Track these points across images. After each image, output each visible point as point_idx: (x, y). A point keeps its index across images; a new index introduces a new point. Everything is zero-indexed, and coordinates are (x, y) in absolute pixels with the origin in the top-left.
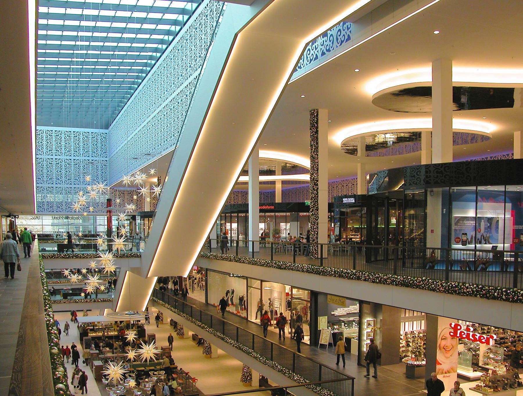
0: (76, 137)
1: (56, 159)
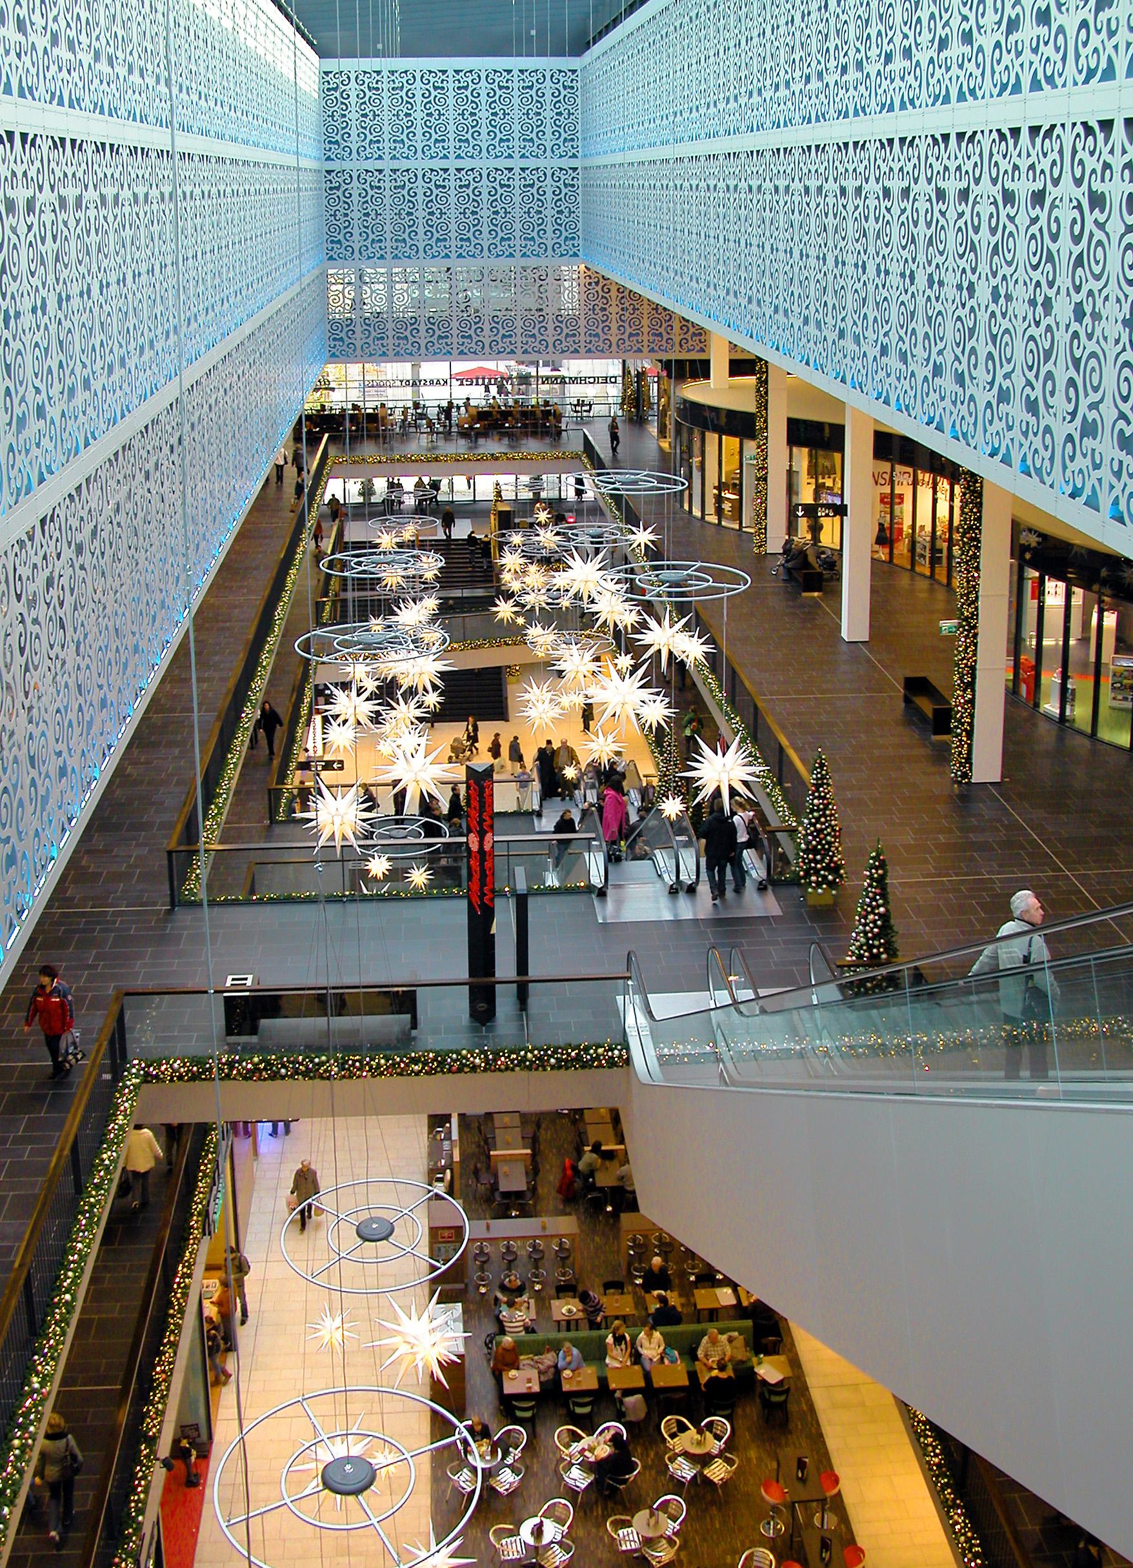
0: (466, 88)
1: (523, 169)
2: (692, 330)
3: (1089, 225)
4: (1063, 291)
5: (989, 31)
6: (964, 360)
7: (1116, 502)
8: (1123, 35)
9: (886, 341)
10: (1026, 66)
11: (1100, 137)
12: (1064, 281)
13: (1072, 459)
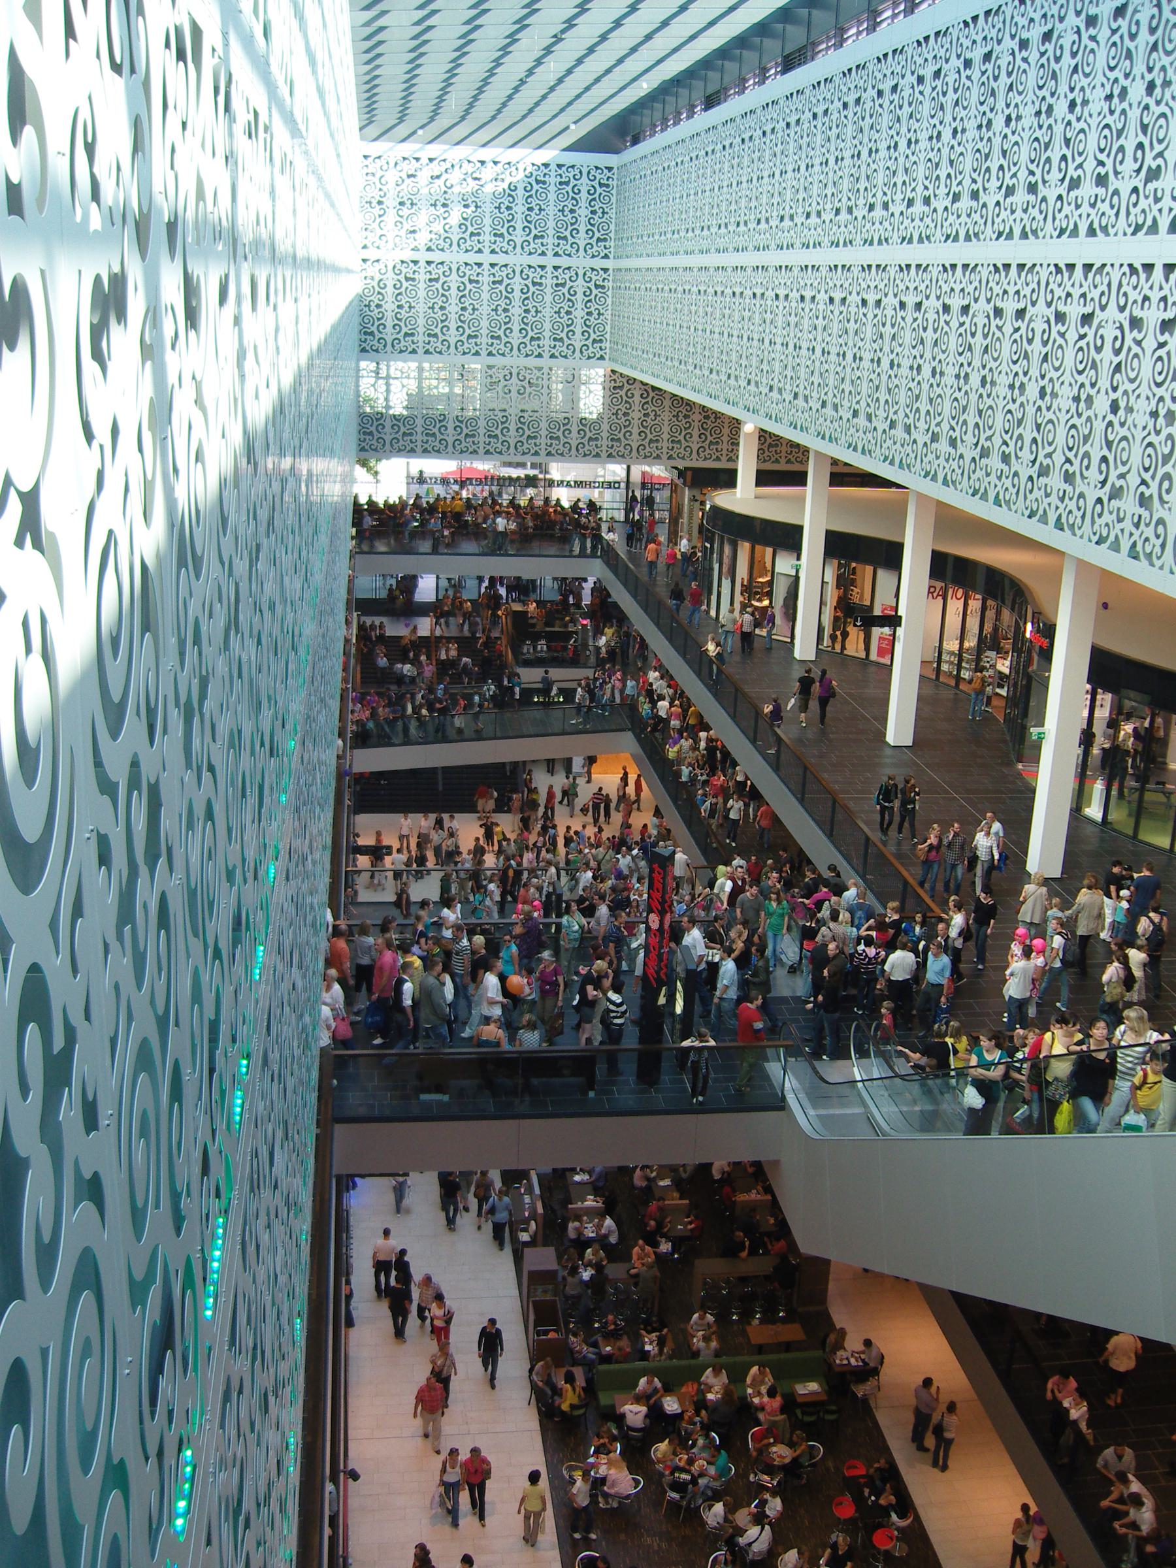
2: (769, 441)
3: (1054, 334)
4: (1103, 391)
5: (1053, 186)
6: (911, 416)
7: (1134, 545)
8: (1167, 202)
9: (857, 407)
10: (1018, 221)
11: (1066, 275)
12: (1104, 383)
13: (1031, 492)
